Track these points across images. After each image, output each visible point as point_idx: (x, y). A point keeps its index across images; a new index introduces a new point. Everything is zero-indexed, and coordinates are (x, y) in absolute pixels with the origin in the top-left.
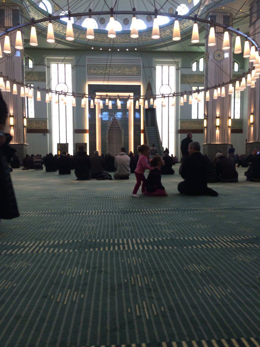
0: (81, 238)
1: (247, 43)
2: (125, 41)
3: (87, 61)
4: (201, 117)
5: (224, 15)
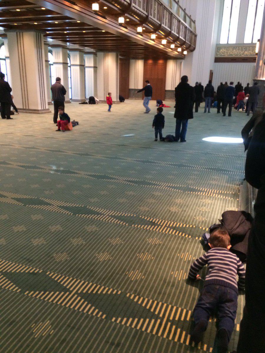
0: (186, 193)
4: (255, 41)
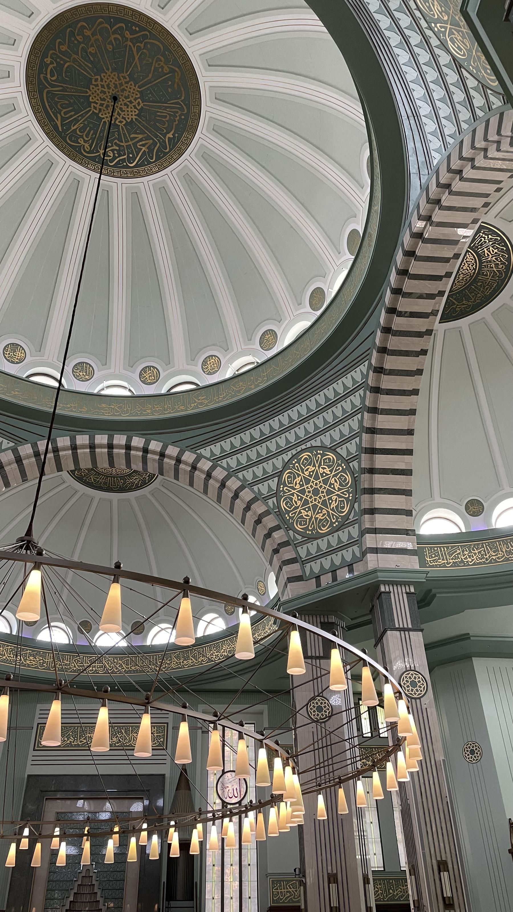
1: (278, 762)
2: (133, 668)
3: (37, 716)
5: (322, 620)
